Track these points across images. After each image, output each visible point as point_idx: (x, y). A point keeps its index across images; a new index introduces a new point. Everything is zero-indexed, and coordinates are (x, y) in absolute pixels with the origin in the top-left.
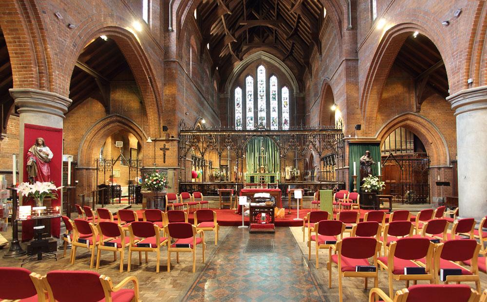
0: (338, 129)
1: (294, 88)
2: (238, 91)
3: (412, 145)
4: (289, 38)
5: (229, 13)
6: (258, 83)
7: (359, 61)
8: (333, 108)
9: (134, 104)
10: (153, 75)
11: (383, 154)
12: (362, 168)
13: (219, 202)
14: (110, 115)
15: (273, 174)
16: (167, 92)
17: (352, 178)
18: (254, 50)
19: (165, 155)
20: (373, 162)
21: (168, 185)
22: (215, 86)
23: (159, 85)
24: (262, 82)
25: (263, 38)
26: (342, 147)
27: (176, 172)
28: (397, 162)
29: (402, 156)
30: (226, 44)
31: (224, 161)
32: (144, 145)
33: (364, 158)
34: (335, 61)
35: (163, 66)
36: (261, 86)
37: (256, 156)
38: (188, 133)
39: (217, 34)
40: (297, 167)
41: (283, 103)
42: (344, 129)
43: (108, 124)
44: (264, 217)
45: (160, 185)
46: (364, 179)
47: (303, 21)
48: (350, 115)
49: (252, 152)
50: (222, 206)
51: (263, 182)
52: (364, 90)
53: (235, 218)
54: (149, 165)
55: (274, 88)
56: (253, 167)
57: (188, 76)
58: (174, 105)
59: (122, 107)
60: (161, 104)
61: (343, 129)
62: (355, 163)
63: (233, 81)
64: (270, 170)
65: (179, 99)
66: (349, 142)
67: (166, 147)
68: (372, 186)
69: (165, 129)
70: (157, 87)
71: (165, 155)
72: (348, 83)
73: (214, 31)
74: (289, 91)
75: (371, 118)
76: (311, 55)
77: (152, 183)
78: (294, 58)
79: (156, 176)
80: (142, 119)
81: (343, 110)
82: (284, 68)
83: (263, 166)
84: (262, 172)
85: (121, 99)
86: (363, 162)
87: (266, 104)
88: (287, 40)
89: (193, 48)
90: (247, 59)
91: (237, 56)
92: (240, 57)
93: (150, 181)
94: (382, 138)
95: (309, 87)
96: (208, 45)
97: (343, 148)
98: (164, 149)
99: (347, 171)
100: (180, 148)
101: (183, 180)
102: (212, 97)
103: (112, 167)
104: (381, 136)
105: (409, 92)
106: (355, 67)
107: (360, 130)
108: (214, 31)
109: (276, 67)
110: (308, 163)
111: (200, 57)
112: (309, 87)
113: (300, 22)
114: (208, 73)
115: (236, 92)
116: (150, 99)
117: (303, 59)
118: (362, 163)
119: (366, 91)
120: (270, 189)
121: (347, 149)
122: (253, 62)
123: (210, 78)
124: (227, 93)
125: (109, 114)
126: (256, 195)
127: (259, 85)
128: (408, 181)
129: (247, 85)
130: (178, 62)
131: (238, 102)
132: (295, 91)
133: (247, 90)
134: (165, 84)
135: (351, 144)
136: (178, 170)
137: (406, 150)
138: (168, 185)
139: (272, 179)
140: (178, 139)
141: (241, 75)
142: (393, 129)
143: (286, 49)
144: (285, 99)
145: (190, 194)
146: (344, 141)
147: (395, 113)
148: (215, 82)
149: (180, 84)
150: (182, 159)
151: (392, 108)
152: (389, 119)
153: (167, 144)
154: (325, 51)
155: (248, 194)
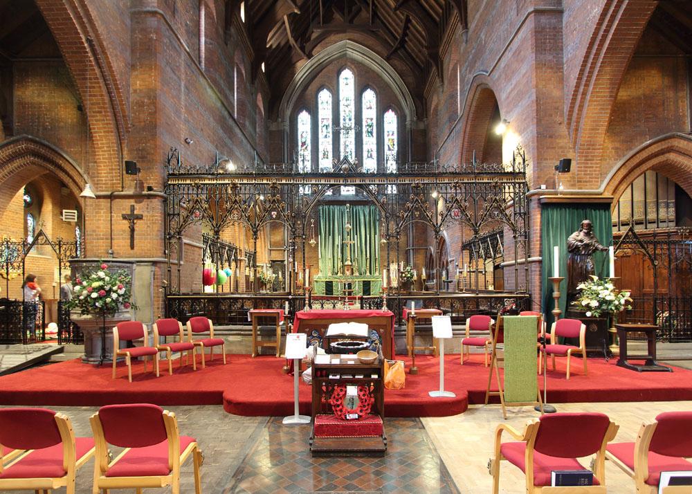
0: (517, 171)
1: (407, 112)
2: (304, 119)
3: (672, 210)
4: (400, 6)
5: (296, 11)
6: (341, 103)
7: (565, 15)
8: (499, 129)
9: (66, 114)
10: (97, 36)
11: (615, 231)
12: (573, 260)
13: (251, 338)
14: (14, 138)
15: (368, 276)
16: (139, 82)
17: (548, 285)
18: (333, 37)
19: (132, 230)
20: (600, 247)
21: (131, 300)
22: (261, 104)
23: (117, 64)
24: (348, 102)
25: (349, 14)
26: (525, 214)
27: (157, 269)
28: (643, 247)
29: (655, 235)
30: (279, 17)
31: (277, 252)
32: (88, 208)
33: (577, 237)
34: (504, 26)
35: (128, 21)
36: (347, 109)
37: (336, 243)
38: (186, 179)
39: (279, 44)
40: (412, 265)
41: (387, 142)
42: (529, 172)
43: (11, 159)
44: (352, 399)
45: (108, 300)
46: (581, 286)
47: (414, 27)
48: (543, 139)
49: (329, 235)
50: (259, 349)
51: (350, 294)
52: (580, 79)
53: (271, 392)
54: (97, 249)
55: (369, 114)
56: (330, 265)
57: (194, 59)
58: (153, 114)
59: (38, 118)
60: (123, 110)
61: (527, 171)
62: (556, 250)
63: (294, 99)
64: (363, 270)
65: (167, 102)
66: (543, 201)
67: (135, 212)
68: (603, 302)
69: (131, 168)
70: (110, 67)
71: (132, 230)
72: (539, 65)
73: (272, 41)
74: (398, 118)
75: (591, 145)
76: (441, 39)
77: (89, 296)
78: (410, 55)
79: (100, 279)
80: (81, 147)
81: (525, 129)
82: (387, 73)
83: (348, 263)
84: (348, 273)
85: (37, 100)
86: (577, 247)
87: (356, 144)
88: (396, 9)
89: (207, 7)
90: (322, 54)
91: (302, 48)
92: (307, 51)
93: (85, 292)
94: (614, 192)
95: (437, 106)
96: (263, 65)
97: (526, 216)
98: (132, 218)
99: (535, 268)
100: (168, 216)
101: (174, 289)
102: (254, 124)
103: (23, 259)
104: (612, 188)
105: (675, 86)
106: (555, 28)
107: (569, 171)
108: (272, 41)
109: (374, 71)
110: (434, 255)
111: (225, 33)
112: (437, 106)
113: (408, 28)
114: (244, 72)
115: (299, 120)
116: (96, 97)
117: (426, 47)
118: (573, 250)
119: (589, 65)
120: (366, 311)
121: (537, 217)
122: (331, 62)
123: (248, 84)
124: (283, 121)
125: (12, 135)
126: (334, 329)
127: (342, 108)
128: (664, 290)
129: (320, 106)
130: (162, 15)
131: (304, 140)
132: (408, 119)
133: (320, 117)
134: (133, 67)
135: (545, 206)
136: (162, 265)
137: (657, 221)
138: (131, 300)
139: (367, 286)
140: (162, 194)
141: (310, 88)
142: (638, 171)
143: (393, 35)
144: (391, 133)
145: (180, 323)
146: (529, 199)
147: (643, 135)
148: (259, 97)
149: (168, 69)
150: (173, 241)
151: (638, 124)
152: (631, 149)
153: (137, 206)
154: (478, 16)
155: (313, 323)
